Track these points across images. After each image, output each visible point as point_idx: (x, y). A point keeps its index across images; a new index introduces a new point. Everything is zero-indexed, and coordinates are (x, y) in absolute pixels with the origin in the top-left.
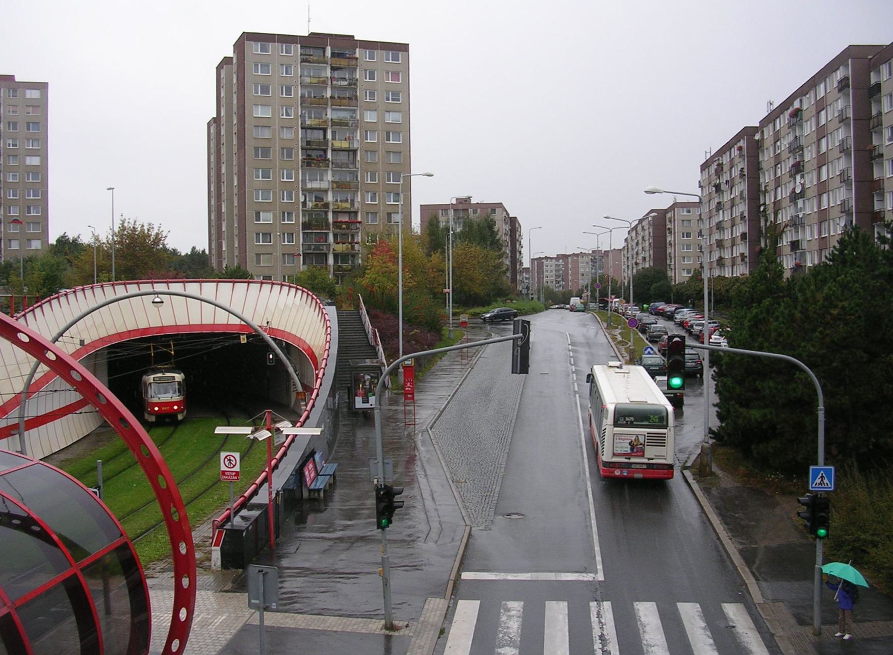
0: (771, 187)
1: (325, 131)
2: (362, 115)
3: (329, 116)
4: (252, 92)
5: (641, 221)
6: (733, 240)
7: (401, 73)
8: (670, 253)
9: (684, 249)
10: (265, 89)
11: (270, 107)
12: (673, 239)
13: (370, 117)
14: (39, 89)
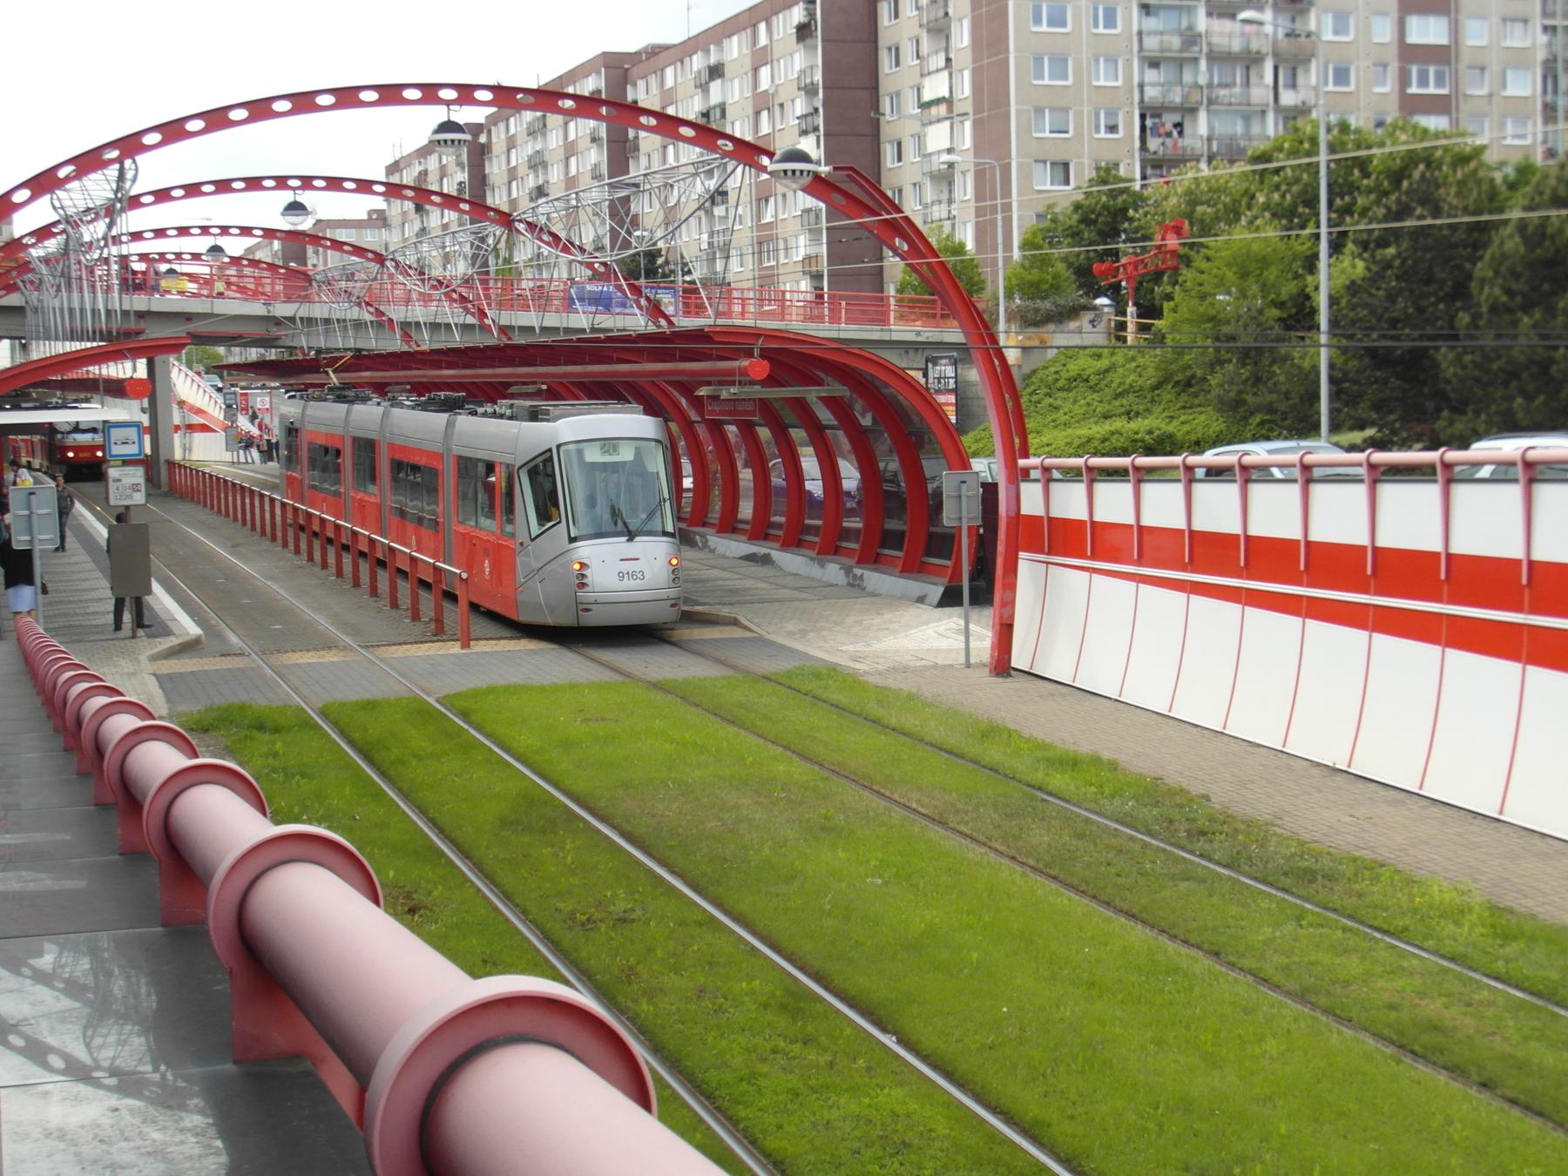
9: (1037, 20)
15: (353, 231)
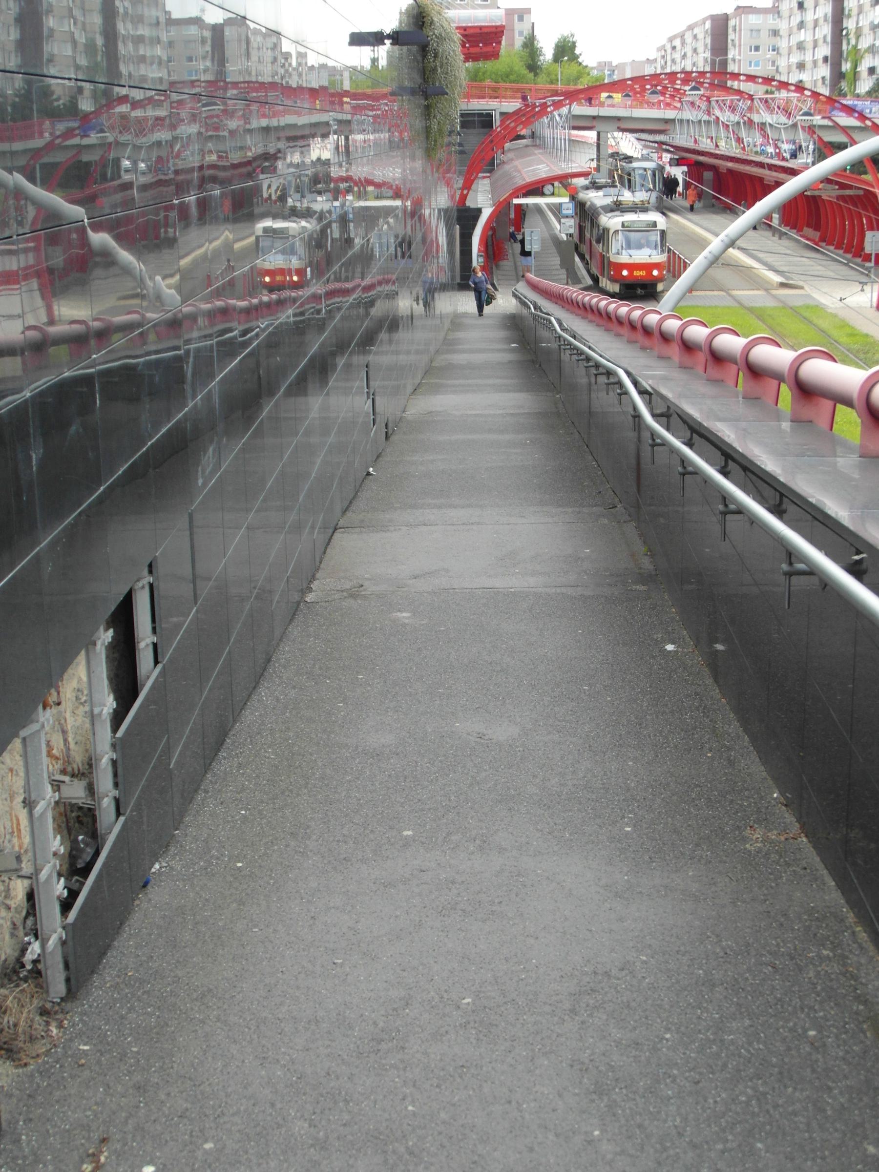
0: (854, 12)
5: (691, 28)
6: (790, 48)
15: (761, 16)
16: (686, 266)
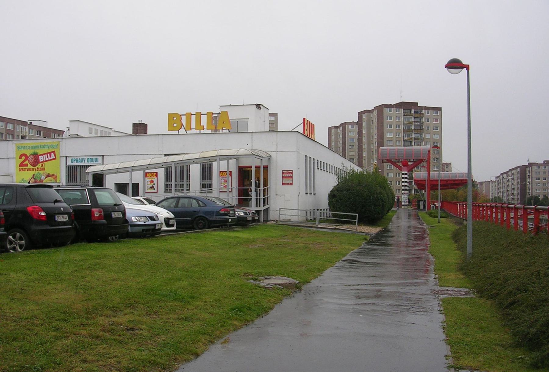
1: (411, 142)
2: (425, 136)
3: (413, 136)
4: (386, 128)
5: (511, 170)
7: (439, 119)
8: (529, 187)
10: (390, 126)
11: (392, 133)
12: (531, 180)
13: (428, 137)
14: (274, 116)
16: (383, 146)
